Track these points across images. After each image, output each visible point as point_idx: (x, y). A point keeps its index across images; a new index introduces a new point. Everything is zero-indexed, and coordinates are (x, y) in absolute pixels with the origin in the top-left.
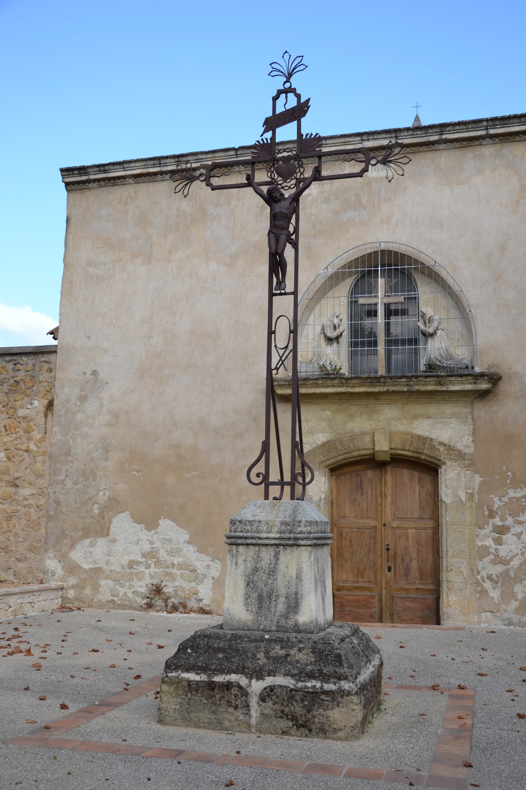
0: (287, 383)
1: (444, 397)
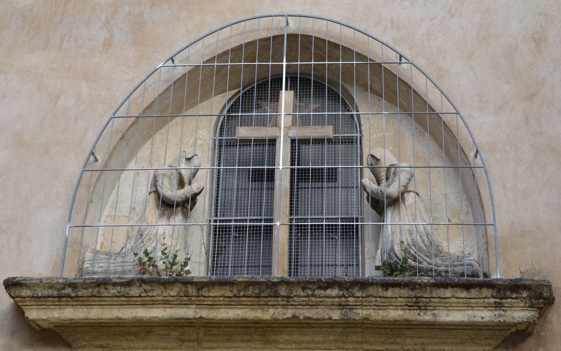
0: (55, 293)
1: (425, 341)
